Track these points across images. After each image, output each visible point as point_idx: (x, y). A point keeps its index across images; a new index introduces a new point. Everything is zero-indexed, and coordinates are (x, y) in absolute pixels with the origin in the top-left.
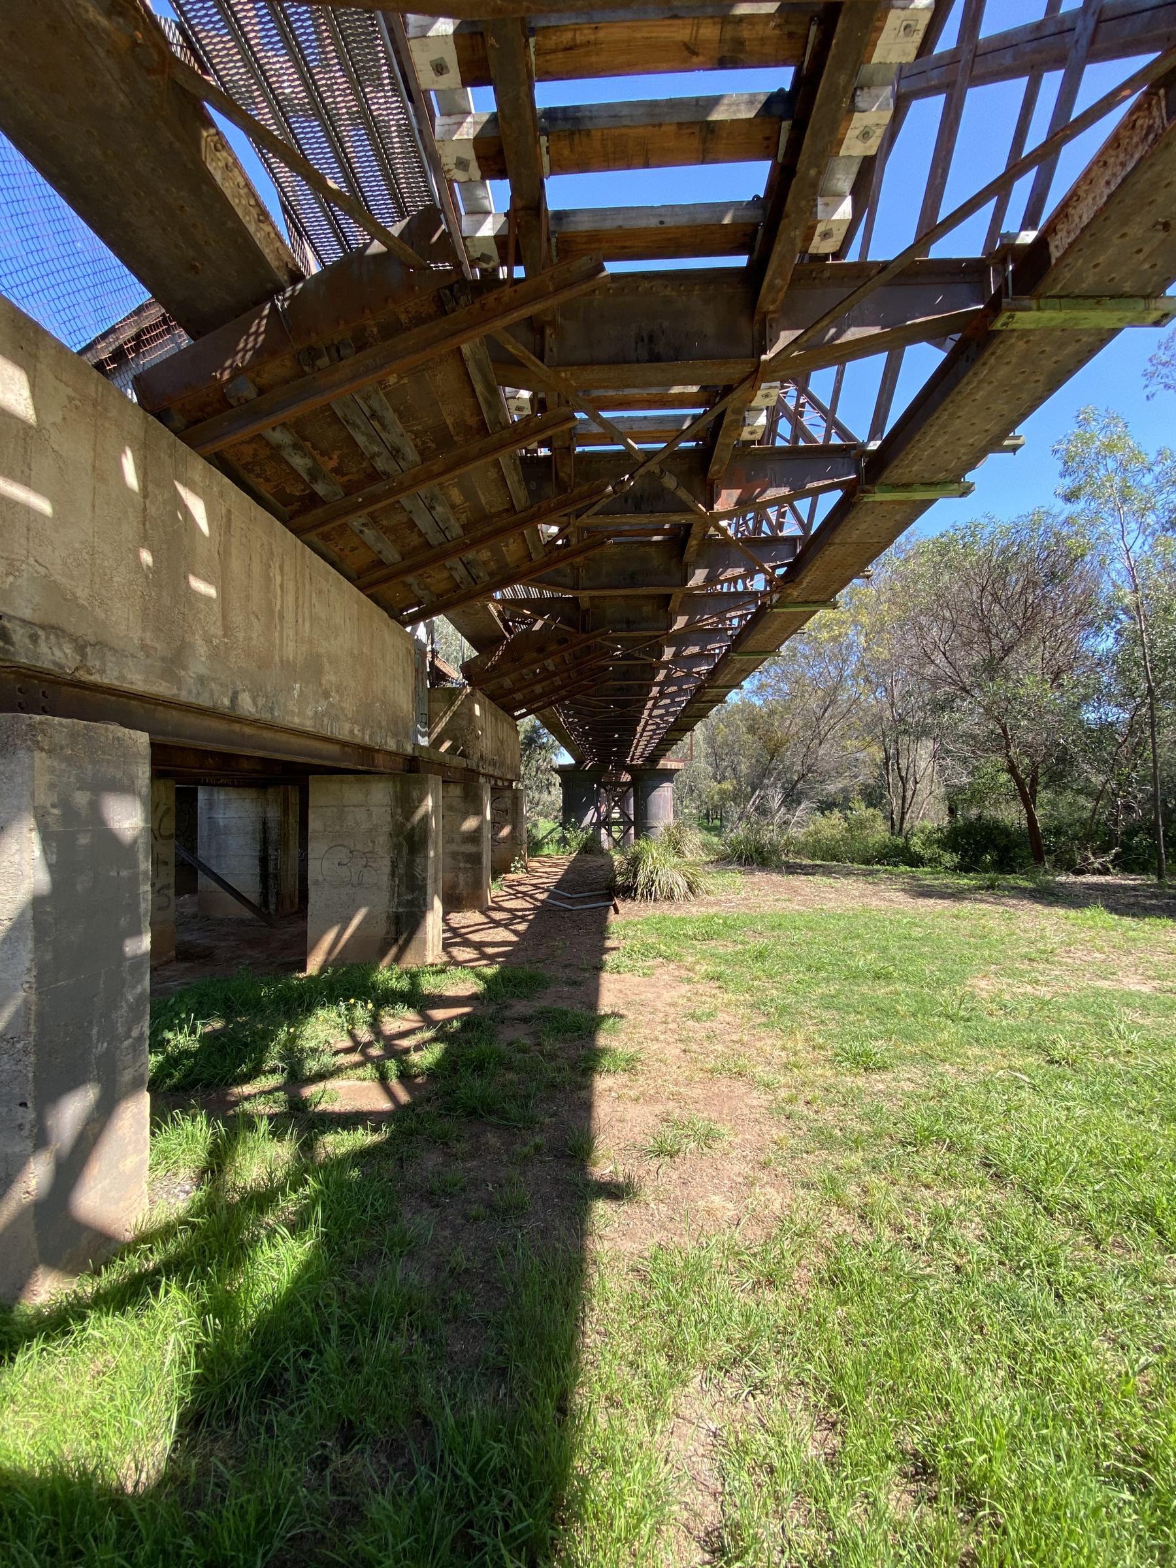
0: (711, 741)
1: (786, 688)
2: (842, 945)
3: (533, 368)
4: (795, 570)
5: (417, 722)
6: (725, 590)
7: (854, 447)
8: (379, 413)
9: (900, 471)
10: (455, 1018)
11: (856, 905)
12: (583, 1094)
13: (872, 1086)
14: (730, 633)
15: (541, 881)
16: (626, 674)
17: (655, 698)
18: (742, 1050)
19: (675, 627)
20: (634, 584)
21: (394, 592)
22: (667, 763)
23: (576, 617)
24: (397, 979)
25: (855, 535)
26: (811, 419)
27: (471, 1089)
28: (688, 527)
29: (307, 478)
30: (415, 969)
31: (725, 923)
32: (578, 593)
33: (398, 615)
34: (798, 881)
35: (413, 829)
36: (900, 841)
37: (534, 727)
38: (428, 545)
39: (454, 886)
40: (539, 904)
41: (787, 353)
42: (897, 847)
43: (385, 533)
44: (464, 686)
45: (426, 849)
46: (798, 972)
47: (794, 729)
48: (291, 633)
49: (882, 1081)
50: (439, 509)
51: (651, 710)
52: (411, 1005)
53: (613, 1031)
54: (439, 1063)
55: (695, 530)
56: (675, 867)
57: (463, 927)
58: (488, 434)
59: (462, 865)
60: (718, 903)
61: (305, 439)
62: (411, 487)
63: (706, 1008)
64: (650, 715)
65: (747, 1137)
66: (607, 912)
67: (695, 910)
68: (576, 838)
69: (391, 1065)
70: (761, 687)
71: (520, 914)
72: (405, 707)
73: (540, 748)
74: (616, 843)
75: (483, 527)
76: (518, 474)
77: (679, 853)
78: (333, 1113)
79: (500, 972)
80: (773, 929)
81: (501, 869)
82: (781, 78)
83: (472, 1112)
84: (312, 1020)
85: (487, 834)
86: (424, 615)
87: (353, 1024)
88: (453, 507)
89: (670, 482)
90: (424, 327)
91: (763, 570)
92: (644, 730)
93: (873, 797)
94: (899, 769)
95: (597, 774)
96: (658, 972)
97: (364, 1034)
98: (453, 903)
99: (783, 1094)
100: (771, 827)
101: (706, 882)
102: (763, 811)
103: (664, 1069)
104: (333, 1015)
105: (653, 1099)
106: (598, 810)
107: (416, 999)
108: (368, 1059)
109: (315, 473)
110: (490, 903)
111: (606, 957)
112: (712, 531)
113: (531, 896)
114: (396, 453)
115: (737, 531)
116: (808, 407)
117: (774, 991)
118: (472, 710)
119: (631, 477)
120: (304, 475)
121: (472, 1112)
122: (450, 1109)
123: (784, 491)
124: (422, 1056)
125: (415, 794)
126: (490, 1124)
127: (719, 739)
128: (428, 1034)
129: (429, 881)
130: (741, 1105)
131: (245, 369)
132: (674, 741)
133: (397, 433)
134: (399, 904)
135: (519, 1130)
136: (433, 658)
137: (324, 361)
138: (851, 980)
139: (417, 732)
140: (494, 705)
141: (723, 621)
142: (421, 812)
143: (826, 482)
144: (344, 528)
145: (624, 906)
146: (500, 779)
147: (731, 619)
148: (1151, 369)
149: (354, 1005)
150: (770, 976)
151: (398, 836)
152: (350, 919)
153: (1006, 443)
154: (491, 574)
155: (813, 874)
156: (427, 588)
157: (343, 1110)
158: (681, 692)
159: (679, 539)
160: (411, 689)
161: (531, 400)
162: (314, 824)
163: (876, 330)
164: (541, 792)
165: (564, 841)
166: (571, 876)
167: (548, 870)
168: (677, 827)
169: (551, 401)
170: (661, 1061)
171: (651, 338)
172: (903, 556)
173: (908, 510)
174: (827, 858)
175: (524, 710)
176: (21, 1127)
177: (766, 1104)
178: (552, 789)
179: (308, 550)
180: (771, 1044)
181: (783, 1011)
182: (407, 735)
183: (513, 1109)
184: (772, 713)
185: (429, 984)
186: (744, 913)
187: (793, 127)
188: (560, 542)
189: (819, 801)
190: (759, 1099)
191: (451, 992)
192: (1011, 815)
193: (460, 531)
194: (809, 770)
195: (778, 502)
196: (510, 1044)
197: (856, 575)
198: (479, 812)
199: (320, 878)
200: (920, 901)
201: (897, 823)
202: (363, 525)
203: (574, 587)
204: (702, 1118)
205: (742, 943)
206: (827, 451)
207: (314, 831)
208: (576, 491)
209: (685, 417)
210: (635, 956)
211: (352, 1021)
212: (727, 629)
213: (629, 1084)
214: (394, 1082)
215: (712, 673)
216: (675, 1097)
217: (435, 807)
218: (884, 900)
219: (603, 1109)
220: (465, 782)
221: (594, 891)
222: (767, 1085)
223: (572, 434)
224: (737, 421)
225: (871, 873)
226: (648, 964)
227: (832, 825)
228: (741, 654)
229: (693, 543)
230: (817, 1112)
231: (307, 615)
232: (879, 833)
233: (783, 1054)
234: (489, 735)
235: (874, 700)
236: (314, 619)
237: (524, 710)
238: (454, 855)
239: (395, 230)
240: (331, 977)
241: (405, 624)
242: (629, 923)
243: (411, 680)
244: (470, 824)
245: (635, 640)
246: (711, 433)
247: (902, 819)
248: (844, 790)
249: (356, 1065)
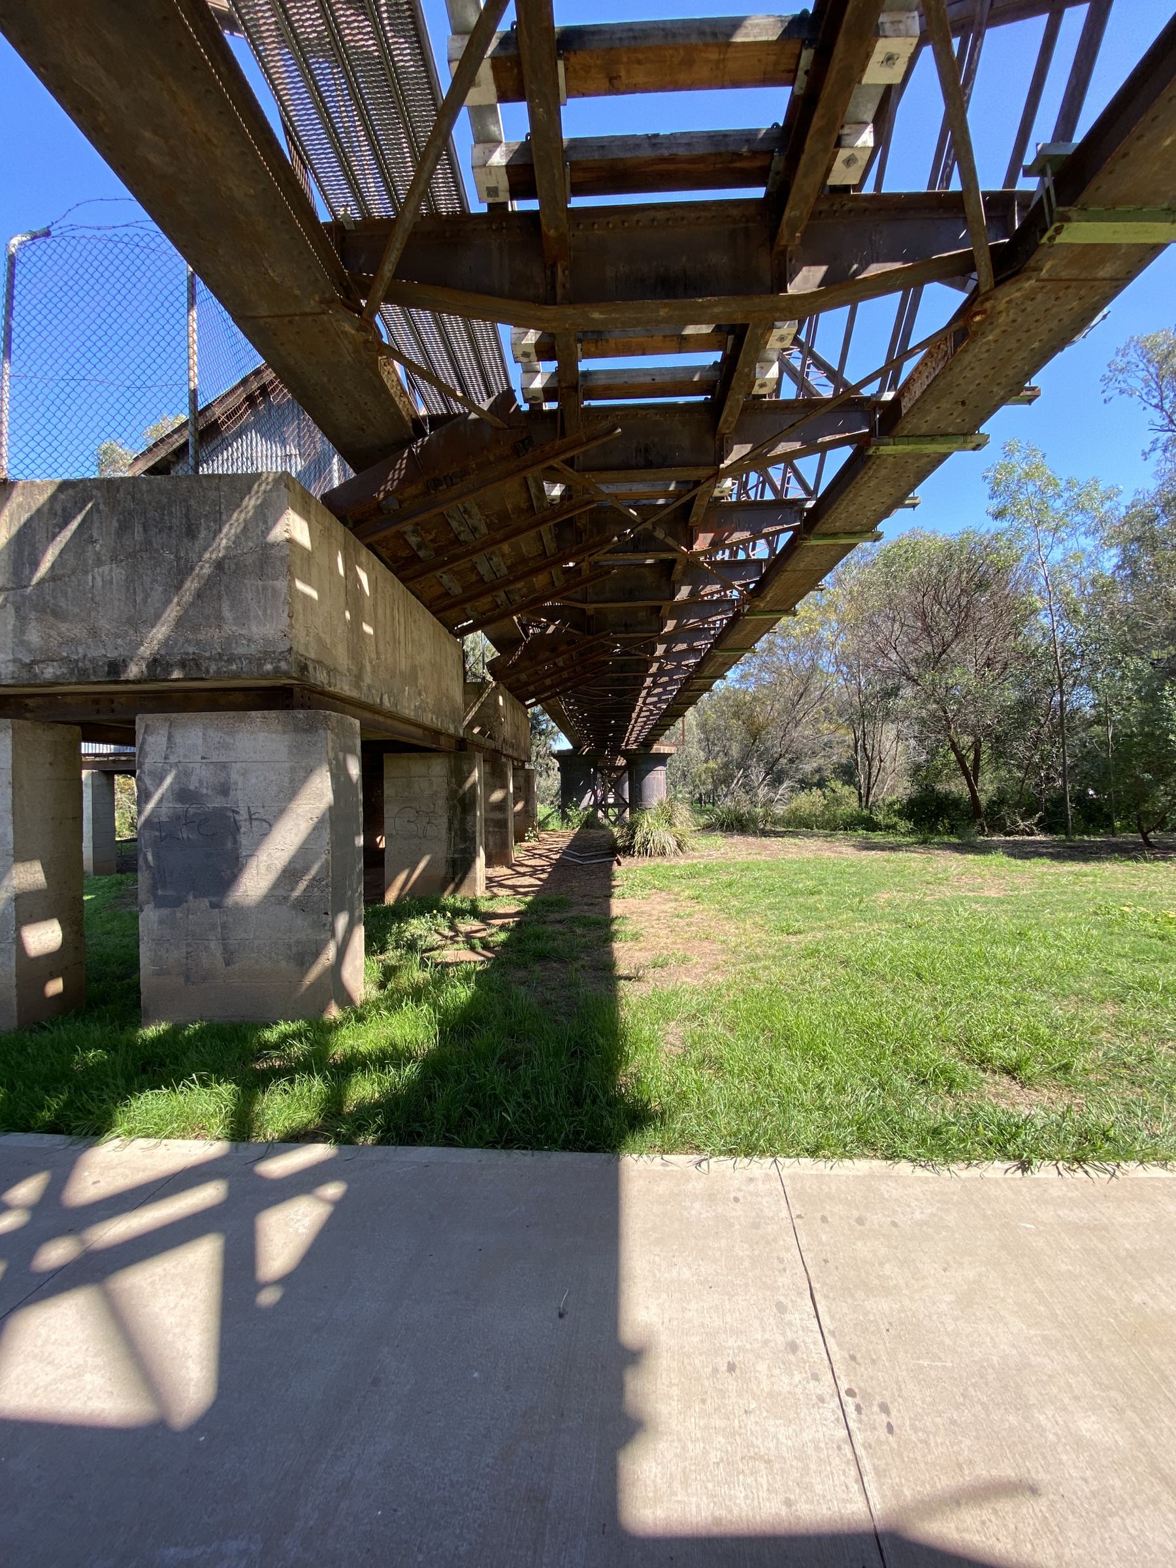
0: (703, 726)
14: (712, 632)
19: (666, 630)
22: (659, 748)
25: (802, 565)
26: (816, 378)
34: (766, 841)
36: (866, 812)
45: (475, 810)
48: (403, 652)
50: (495, 559)
51: (645, 698)
60: (702, 857)
62: (482, 549)
64: (644, 703)
73: (540, 734)
75: (522, 569)
81: (520, 838)
82: (717, 356)
92: (638, 716)
93: (847, 773)
95: (594, 759)
101: (691, 842)
106: (594, 793)
116: (813, 368)
118: (497, 701)
123: (746, 535)
125: (465, 767)
131: (394, 492)
132: (667, 727)
142: (470, 781)
145: (626, 861)
148: (1108, 374)
174: (799, 825)
176: (324, 925)
178: (551, 772)
187: (735, 339)
192: (957, 787)
195: (744, 542)
198: (505, 786)
200: (864, 853)
212: (711, 629)
221: (593, 859)
227: (809, 801)
228: (722, 650)
229: (679, 568)
232: (852, 805)
239: (485, 406)
244: (497, 796)
247: (868, 793)
248: (819, 770)
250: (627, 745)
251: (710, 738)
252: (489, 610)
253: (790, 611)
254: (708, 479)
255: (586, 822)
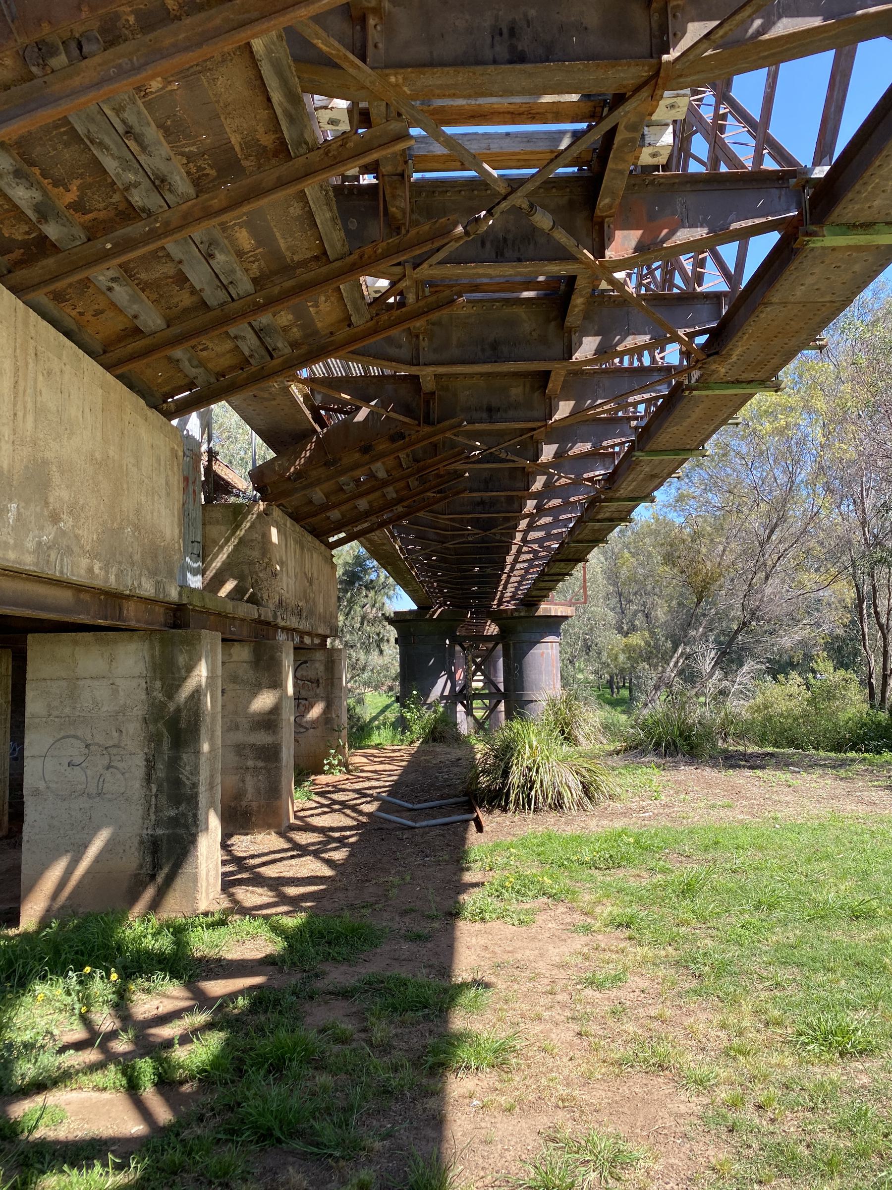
0: (613, 576)
1: (716, 499)
2: (803, 869)
3: (351, 70)
4: (719, 338)
5: (186, 553)
6: (626, 364)
7: (793, 174)
8: (137, 129)
9: (857, 207)
10: (241, 992)
11: (822, 810)
12: (431, 1103)
13: (851, 1079)
14: (634, 423)
15: (367, 784)
16: (488, 483)
17: (530, 515)
18: (663, 1029)
19: (557, 417)
20: (496, 359)
21: (153, 370)
23: (418, 405)
24: (154, 935)
25: (799, 292)
26: (735, 134)
27: (265, 1100)
28: (571, 280)
29: (33, 216)
30: (181, 920)
31: (637, 842)
32: (414, 370)
33: (165, 403)
34: (741, 778)
35: (178, 710)
37: (357, 557)
38: (203, 305)
39: (239, 795)
40: (364, 819)
41: (698, 51)
42: (879, 724)
43: (143, 290)
44: (255, 501)
46: (742, 912)
47: (729, 558)
49: (865, 1071)
50: (220, 257)
51: (526, 532)
52: (175, 974)
53: (475, 1007)
54: (216, 1063)
55: (580, 283)
56: (564, 760)
57: (253, 857)
58: (289, 157)
59: (250, 763)
60: (627, 813)
61: (32, 164)
62: (180, 228)
63: (610, 970)
64: (524, 541)
65: (672, 1161)
66: (466, 830)
67: (593, 824)
68: (422, 719)
69: (146, 1067)
70: (680, 499)
71: (337, 835)
72: (168, 533)
74: (479, 725)
75: (283, 281)
76: (331, 210)
77: (569, 738)
78: (57, 1142)
79: (308, 923)
80: (706, 849)
81: (307, 768)
83: (265, 1136)
84: (27, 999)
85: (288, 716)
86: (201, 401)
87: (89, 1005)
88: (240, 254)
89: (543, 220)
90: (203, 15)
91: (676, 339)
92: (516, 561)
93: (843, 653)
94: (876, 612)
96: (540, 918)
97: (105, 1020)
98: (237, 820)
99: (723, 1094)
100: (702, 699)
101: (608, 782)
102: (690, 676)
103: (550, 1062)
104: (59, 992)
105: (534, 1108)
106: (451, 677)
107: (182, 965)
108: (110, 1057)
109: (44, 211)
110: (292, 820)
111: (465, 897)
112: (604, 285)
113: (354, 808)
114: (159, 183)
115: (639, 285)
116: (730, 120)
117: (708, 941)
118: (266, 536)
119: (490, 213)
120: (30, 213)
121: (265, 1136)
122: (232, 1132)
123: (701, 233)
124: (191, 1052)
125: (182, 660)
126: (293, 1153)
127: (624, 572)
128: (201, 1018)
129: (202, 789)
130: (663, 1113)
132: (561, 576)
133: (162, 156)
134: (158, 823)
135: (336, 1160)
136: (210, 461)
137: (60, 60)
138: (817, 921)
139: (185, 568)
140: (298, 528)
141: (625, 406)
142: (190, 685)
143: (757, 221)
144: (87, 283)
146: (309, 634)
147: (635, 404)
149: (90, 976)
150: (702, 919)
151: (156, 721)
152: (86, 846)
153: (730, 421)
154: (294, 345)
155: (762, 767)
156: (201, 364)
157: (71, 1137)
158: (567, 506)
159: (559, 296)
160: (177, 506)
161: (350, 111)
162: (34, 706)
163: (817, 22)
164: (368, 652)
165: (402, 724)
166: (412, 776)
167: (379, 767)
168: (567, 702)
169: (377, 112)
170: (545, 1050)
171: (512, 32)
172: (869, 318)
173: (870, 259)
174: (782, 744)
175: (342, 535)
177: (698, 1110)
178: (385, 647)
179: (33, 315)
180: (703, 1020)
181: (721, 970)
182: (170, 574)
183: (327, 1130)
184: (696, 536)
185: (203, 943)
186: (665, 827)
188: (391, 300)
189: (769, 661)
190: (689, 1103)
191: (233, 953)
193: (248, 286)
194: (753, 616)
196: (322, 1031)
197: (805, 346)
198: (276, 684)
199: (42, 785)
201: (878, 691)
202: (113, 280)
203: (414, 361)
204: (605, 1133)
205: (662, 872)
206: (757, 179)
207: (33, 716)
208: (413, 232)
209: (563, 133)
210: (506, 895)
211: (87, 1000)
212: (629, 419)
213: (498, 1085)
214: (149, 1093)
215: (611, 479)
216: (566, 1103)
217: (211, 678)
218: (862, 802)
219: (461, 1126)
220: (256, 639)
221: (449, 797)
222: (700, 1082)
223: (406, 156)
224: (633, 140)
225: (843, 764)
226: (527, 906)
227: (787, 696)
229: (578, 301)
230: (773, 1121)
231: (30, 405)
232: (853, 705)
233: (722, 1034)
234: (292, 573)
235: (838, 518)
236: (40, 412)
237: (342, 535)
238: (239, 749)
240: (56, 933)
241: (169, 415)
242: (497, 845)
243: (177, 495)
244: (264, 701)
245: (501, 435)
246: (598, 158)
249: (93, 1068)
250: (500, 603)
251: (622, 593)
252: (232, 368)
253: (768, 381)
254: (638, 89)
255: (433, 731)
